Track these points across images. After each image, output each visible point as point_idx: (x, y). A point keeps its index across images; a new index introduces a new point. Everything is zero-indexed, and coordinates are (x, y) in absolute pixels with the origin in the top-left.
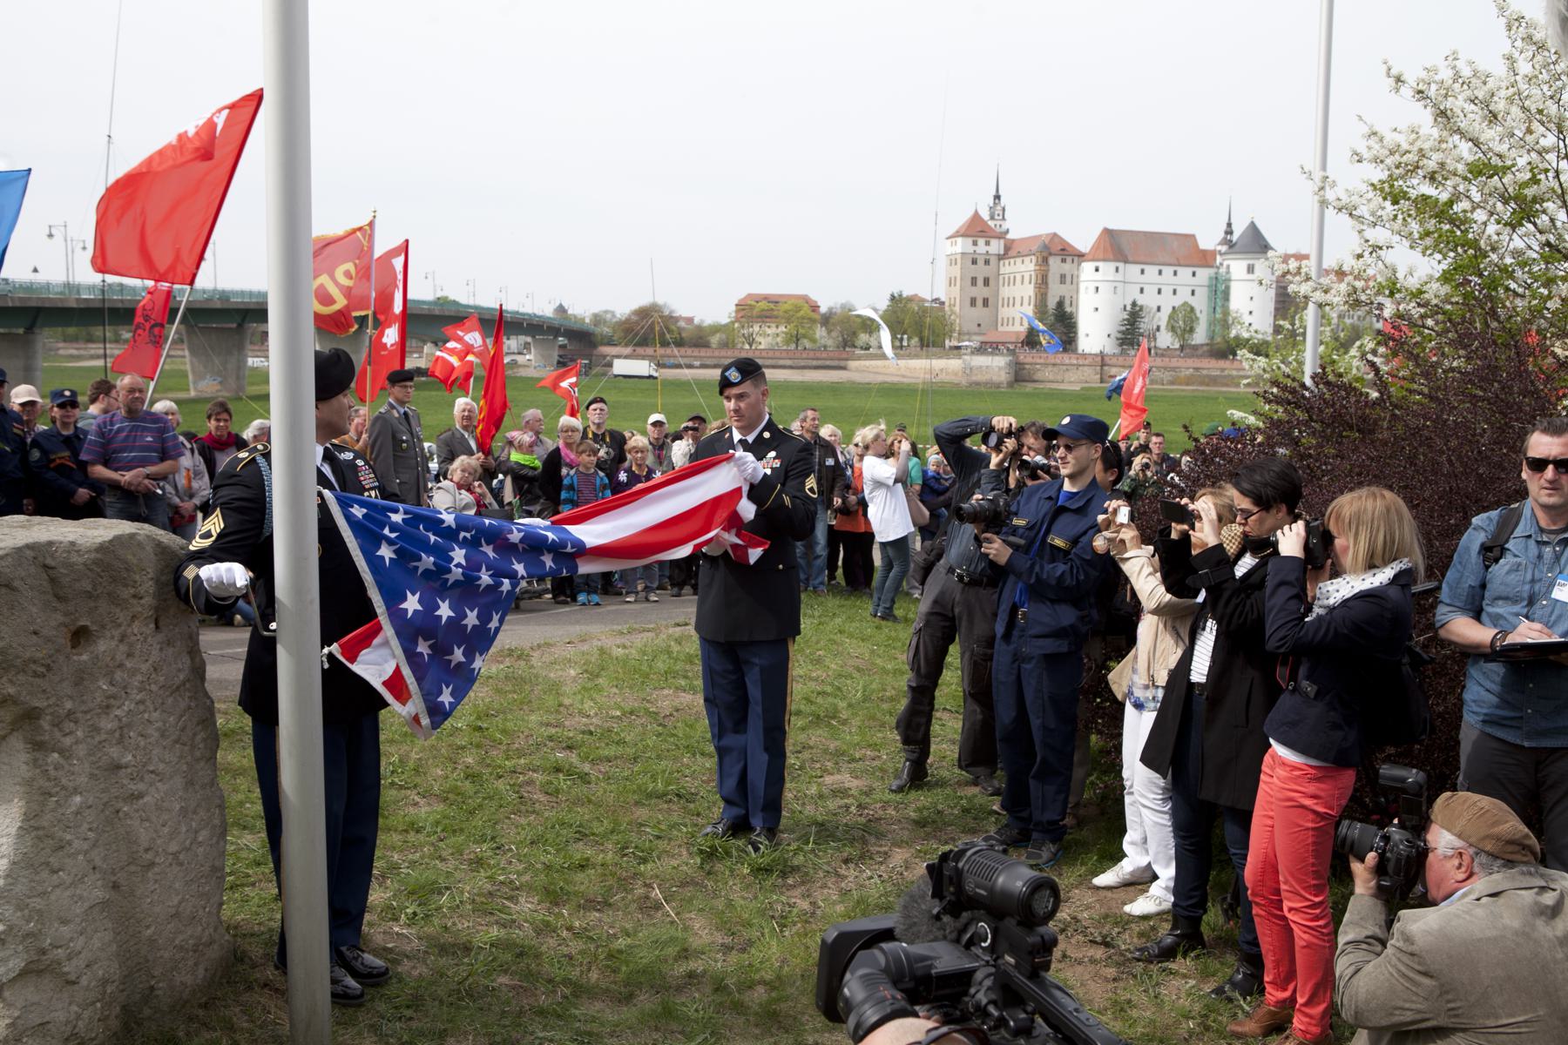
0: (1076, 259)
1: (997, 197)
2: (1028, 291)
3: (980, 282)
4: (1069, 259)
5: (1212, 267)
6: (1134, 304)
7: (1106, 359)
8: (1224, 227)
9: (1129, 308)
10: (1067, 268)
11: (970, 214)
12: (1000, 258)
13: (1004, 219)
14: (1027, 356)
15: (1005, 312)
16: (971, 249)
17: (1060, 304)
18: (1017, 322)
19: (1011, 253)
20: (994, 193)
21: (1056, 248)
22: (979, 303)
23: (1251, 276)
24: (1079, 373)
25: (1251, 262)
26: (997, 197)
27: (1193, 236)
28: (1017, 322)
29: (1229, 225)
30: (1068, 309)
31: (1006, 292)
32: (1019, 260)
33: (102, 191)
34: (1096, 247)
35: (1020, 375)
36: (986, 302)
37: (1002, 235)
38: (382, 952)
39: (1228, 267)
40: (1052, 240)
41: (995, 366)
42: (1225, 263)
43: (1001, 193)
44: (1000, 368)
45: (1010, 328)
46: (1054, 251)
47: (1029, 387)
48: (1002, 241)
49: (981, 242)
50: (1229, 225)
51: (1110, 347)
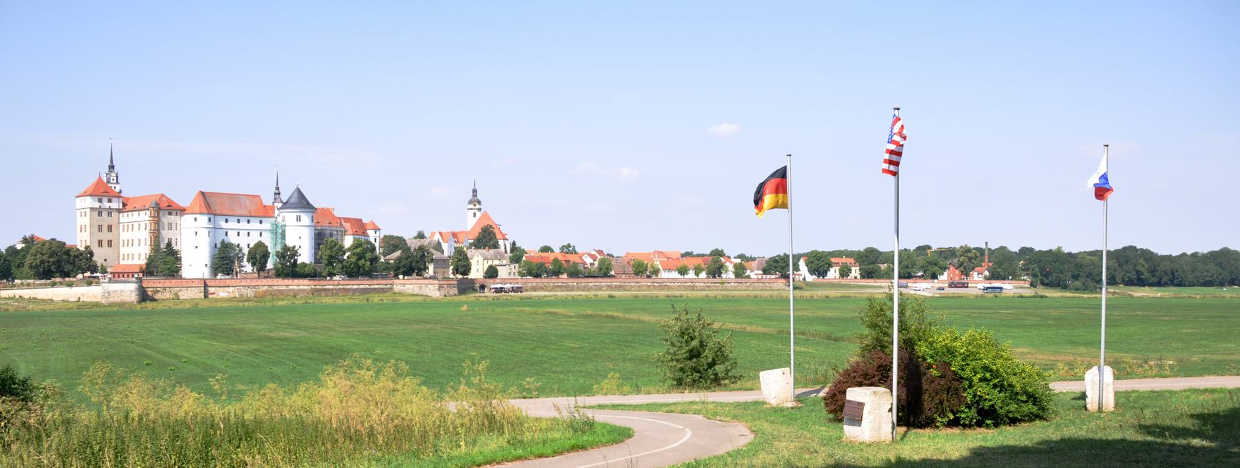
0: (179, 212)
1: (112, 167)
2: (145, 235)
3: (105, 229)
4: (174, 212)
5: (273, 217)
6: (223, 242)
7: (207, 282)
8: (274, 190)
9: (219, 246)
10: (173, 218)
11: (95, 179)
12: (119, 211)
13: (117, 182)
14: (150, 283)
15: (124, 250)
16: (97, 205)
17: (169, 244)
18: (136, 257)
19: (128, 208)
20: (109, 164)
21: (164, 205)
22: (105, 243)
23: (299, 223)
24: (189, 292)
25: (299, 214)
26: (112, 167)
27: (259, 196)
28: (136, 257)
29: (277, 188)
30: (175, 248)
31: (124, 236)
32: (136, 213)
33: (400, 236)
34: (194, 203)
35: (144, 296)
36: (110, 243)
37: (118, 195)
38: (973, 274)
39: (284, 217)
40: (160, 199)
41: (127, 291)
42: (282, 215)
43: (279, 186)
44: (131, 292)
45: (130, 262)
46: (163, 208)
47: (149, 305)
48: (121, 200)
49: (105, 200)
50: (277, 188)
51: (205, 273)
